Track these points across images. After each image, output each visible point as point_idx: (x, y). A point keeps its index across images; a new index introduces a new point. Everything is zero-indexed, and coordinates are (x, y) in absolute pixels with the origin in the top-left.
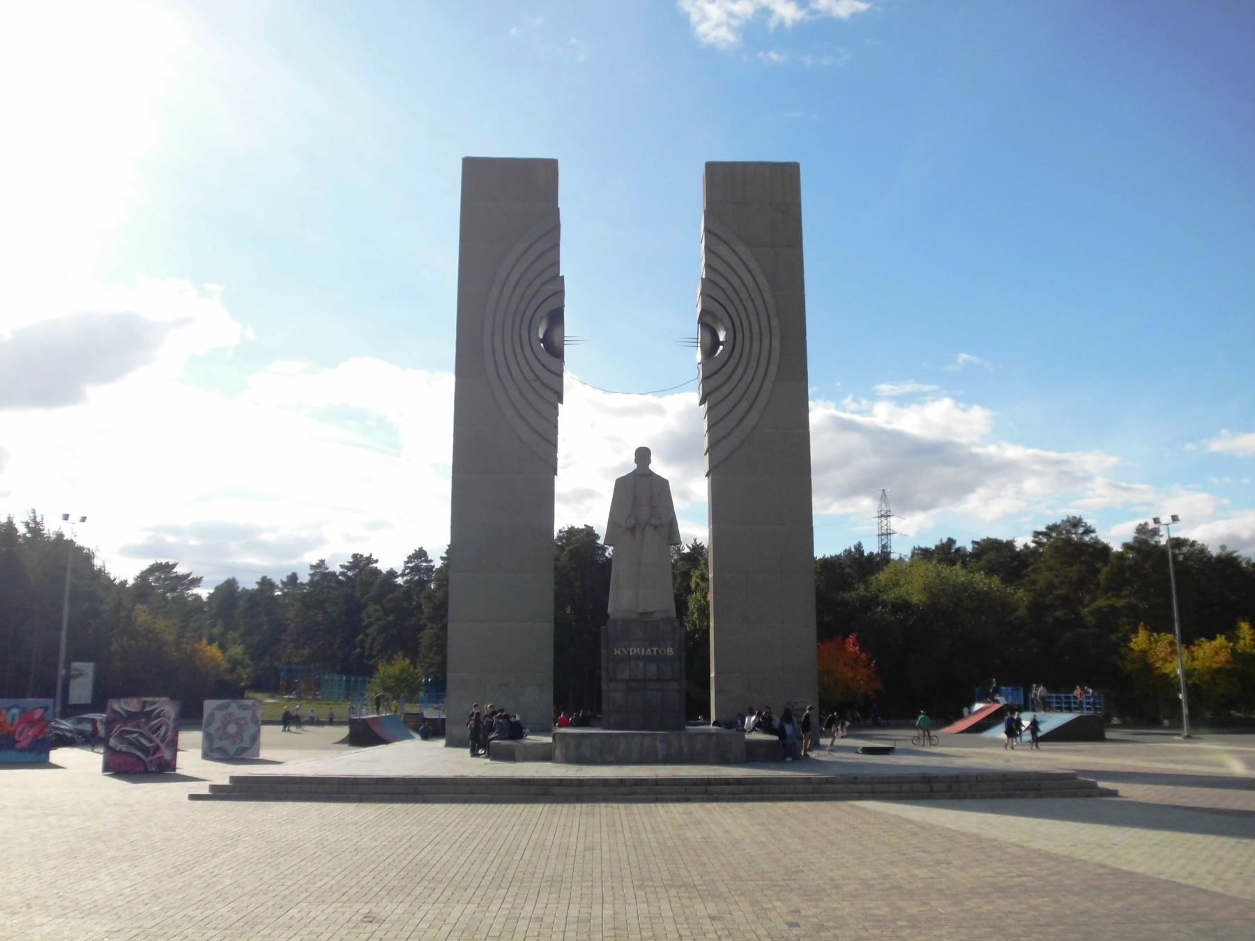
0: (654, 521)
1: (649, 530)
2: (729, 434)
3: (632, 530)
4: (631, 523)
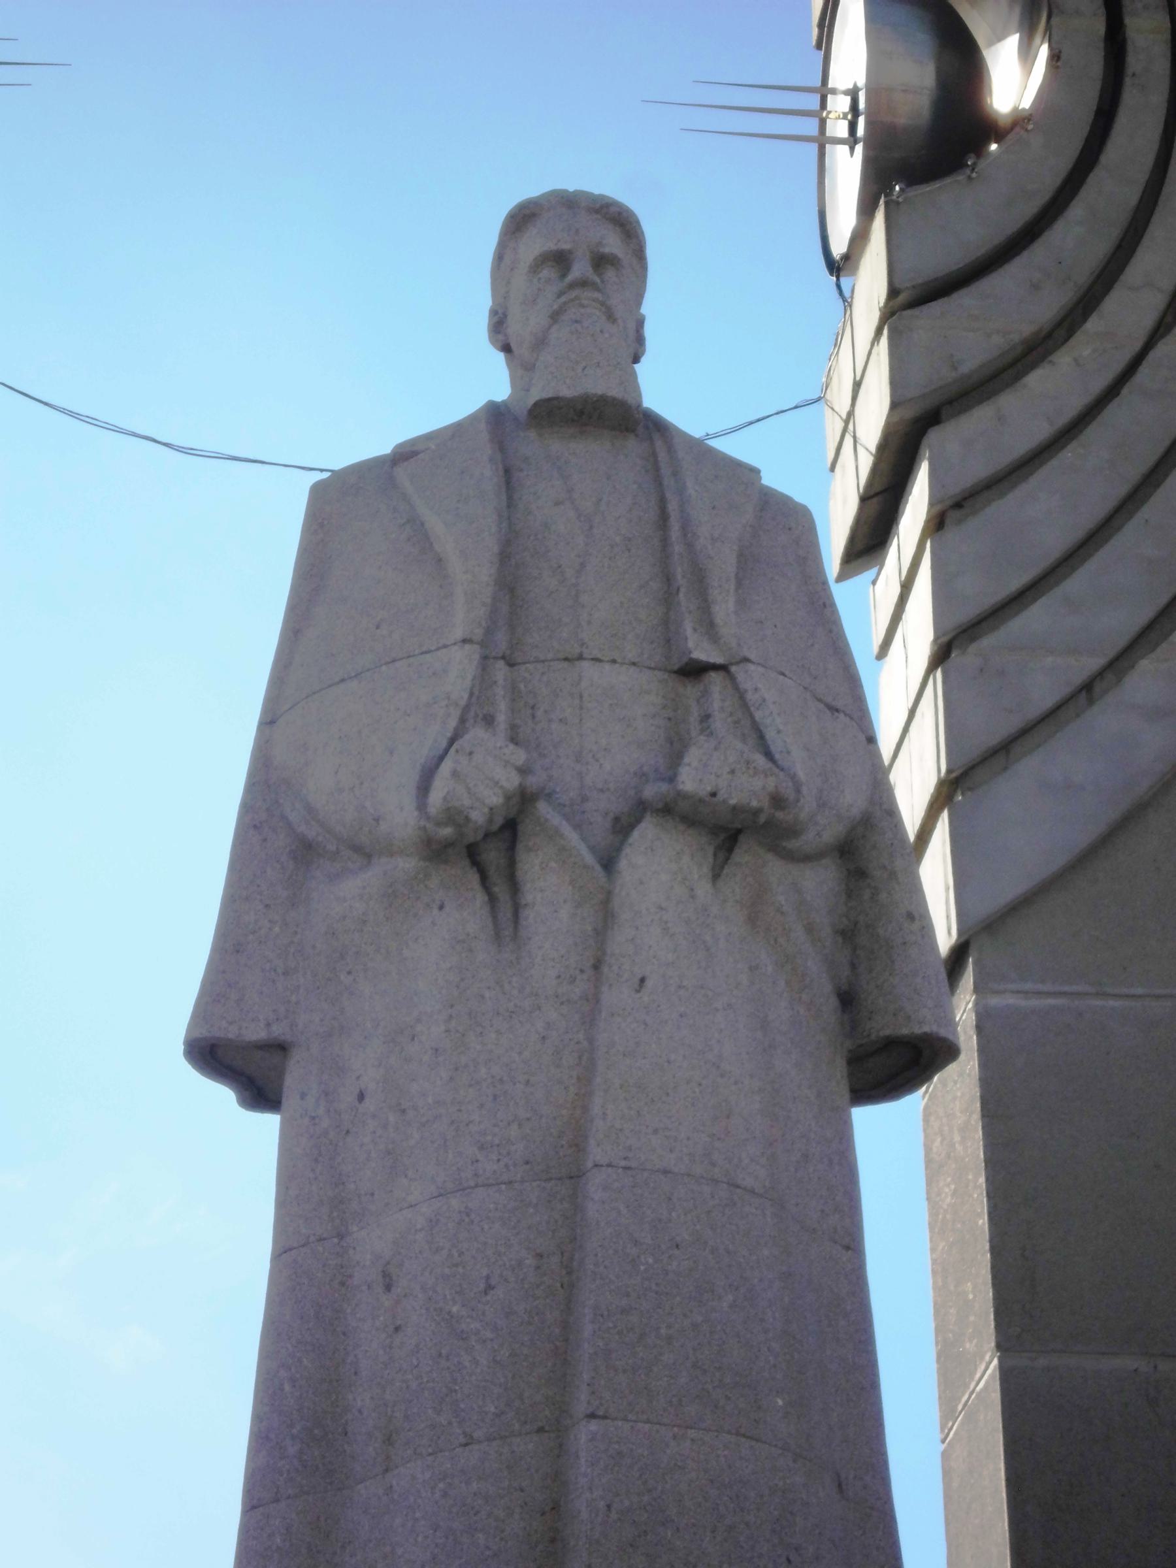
0: (714, 771)
1: (659, 864)
2: (1088, 691)
3: (486, 852)
4: (482, 780)
